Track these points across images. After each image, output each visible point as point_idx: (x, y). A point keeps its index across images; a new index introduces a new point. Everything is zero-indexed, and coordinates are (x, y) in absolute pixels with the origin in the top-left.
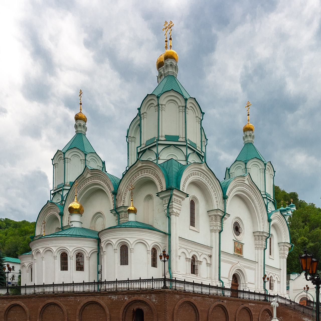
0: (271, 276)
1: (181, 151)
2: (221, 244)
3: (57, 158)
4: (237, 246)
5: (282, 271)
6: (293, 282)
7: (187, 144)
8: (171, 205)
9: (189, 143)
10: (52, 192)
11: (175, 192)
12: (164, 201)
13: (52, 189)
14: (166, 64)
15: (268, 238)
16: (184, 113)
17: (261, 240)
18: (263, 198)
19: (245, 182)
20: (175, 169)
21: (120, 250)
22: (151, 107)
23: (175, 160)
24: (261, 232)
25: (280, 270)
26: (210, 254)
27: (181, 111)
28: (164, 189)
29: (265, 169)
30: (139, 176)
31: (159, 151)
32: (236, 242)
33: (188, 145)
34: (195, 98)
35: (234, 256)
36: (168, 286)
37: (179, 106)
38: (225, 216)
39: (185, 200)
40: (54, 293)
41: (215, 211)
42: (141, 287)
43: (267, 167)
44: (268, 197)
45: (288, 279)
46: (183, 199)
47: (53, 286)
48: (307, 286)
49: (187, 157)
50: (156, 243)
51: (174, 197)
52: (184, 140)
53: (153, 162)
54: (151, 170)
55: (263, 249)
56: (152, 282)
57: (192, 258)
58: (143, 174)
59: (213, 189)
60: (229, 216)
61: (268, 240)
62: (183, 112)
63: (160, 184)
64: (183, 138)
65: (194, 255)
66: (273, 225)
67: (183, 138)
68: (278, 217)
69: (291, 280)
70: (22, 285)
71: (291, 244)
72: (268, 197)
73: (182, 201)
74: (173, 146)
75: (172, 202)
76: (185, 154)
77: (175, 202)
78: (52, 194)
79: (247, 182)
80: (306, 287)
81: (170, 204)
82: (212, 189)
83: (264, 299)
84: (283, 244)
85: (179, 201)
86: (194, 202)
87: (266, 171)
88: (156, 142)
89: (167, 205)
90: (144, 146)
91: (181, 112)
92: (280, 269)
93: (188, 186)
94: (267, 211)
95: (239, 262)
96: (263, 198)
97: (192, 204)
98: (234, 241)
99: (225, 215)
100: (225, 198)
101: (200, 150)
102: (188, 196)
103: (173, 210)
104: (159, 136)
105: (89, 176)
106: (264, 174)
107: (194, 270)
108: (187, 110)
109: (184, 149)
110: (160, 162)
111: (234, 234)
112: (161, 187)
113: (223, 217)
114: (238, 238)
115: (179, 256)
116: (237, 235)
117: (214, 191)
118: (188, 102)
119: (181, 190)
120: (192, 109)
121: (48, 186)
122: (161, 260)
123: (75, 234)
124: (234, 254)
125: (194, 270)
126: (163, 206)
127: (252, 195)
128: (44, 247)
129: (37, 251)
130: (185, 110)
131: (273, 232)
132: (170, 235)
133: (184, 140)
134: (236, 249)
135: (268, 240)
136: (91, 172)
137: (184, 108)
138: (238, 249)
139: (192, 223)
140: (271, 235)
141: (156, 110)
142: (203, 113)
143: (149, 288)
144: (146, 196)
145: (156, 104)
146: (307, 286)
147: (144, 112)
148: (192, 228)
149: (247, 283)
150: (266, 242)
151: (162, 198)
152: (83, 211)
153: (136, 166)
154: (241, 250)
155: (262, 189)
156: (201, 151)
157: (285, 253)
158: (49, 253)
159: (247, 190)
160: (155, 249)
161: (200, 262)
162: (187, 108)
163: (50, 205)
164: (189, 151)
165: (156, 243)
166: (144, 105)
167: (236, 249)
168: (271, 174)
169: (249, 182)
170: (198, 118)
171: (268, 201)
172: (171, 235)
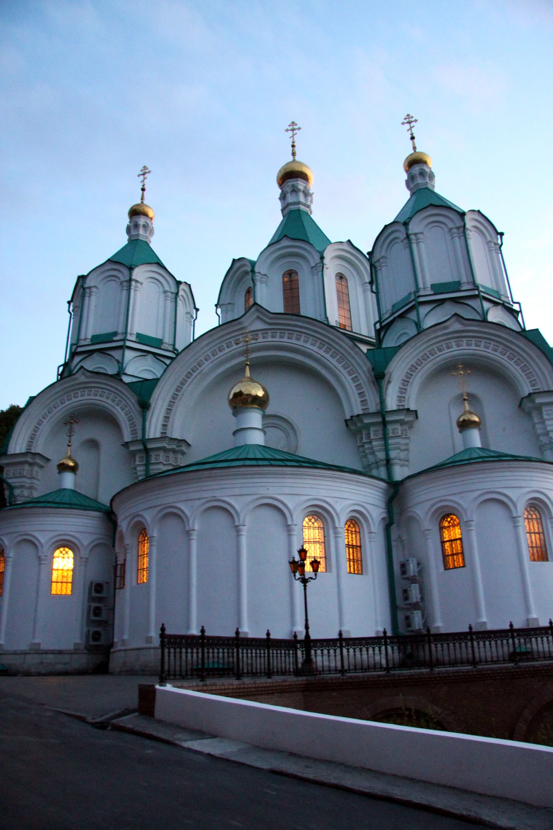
1: (469, 308)
7: (479, 293)
9: (483, 290)
14: (412, 174)
16: (462, 238)
27: (455, 236)
31: (422, 316)
33: (482, 294)
34: (479, 211)
37: (450, 229)
52: (471, 287)
64: (468, 283)
67: (169, 345)
70: (389, 409)
88: (413, 300)
90: (388, 315)
91: (457, 239)
104: (126, 333)
108: (468, 232)
121: (73, 305)
122: (295, 578)
123: (294, 453)
128: (156, 506)
129: (136, 519)
142: (502, 234)
145: (403, 236)
158: (173, 523)
164: (486, 305)
172: (346, 426)
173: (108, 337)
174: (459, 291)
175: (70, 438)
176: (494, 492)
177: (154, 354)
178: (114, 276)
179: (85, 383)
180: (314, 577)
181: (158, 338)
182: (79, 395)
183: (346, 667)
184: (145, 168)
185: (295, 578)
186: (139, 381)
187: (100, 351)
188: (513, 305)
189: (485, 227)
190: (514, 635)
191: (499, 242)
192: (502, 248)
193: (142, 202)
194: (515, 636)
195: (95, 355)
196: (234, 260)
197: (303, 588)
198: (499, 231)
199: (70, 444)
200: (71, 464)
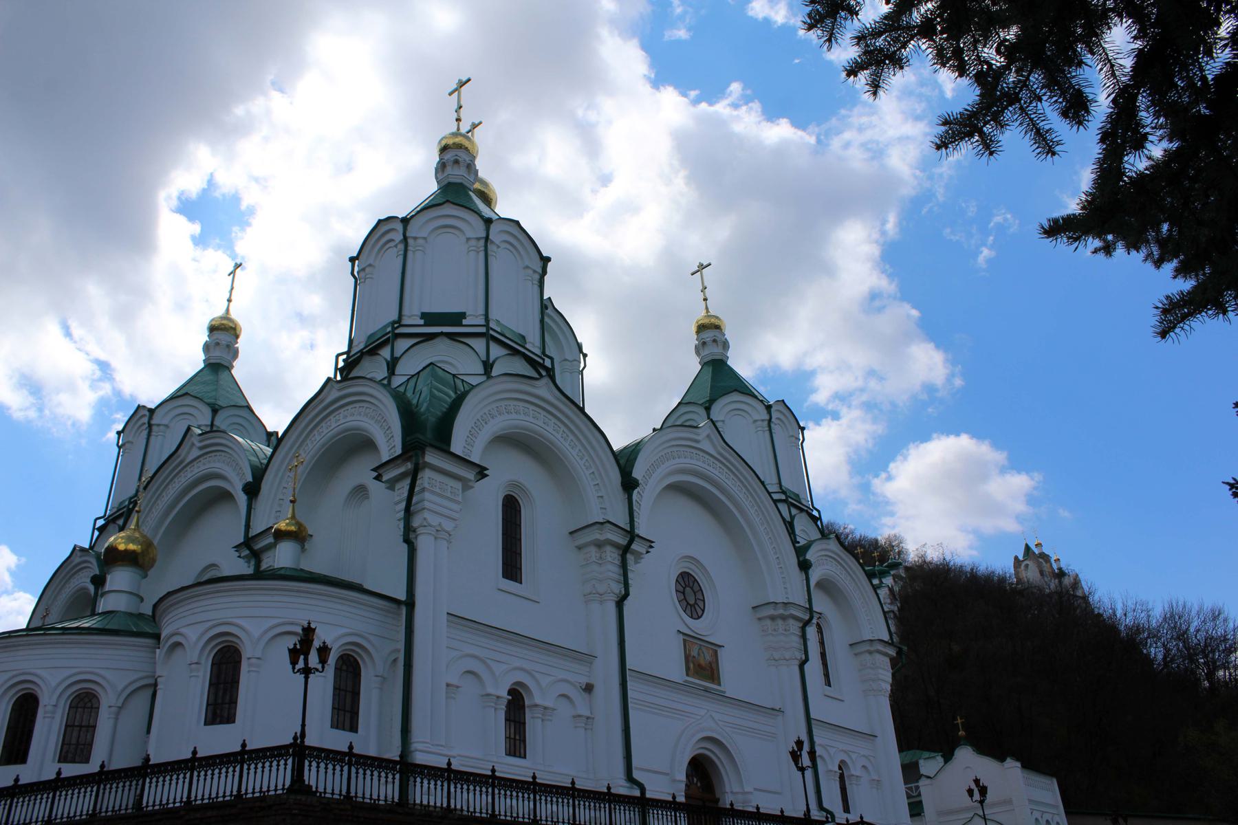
0: (843, 762)
3: (133, 427)
4: (694, 653)
6: (931, 785)
8: (417, 503)
10: (100, 523)
11: (431, 457)
13: (102, 515)
15: (807, 623)
17: (785, 630)
18: (775, 502)
21: (213, 664)
22: (387, 249)
24: (779, 605)
26: (584, 680)
28: (399, 451)
29: (770, 421)
32: (689, 640)
33: (491, 332)
34: (517, 223)
35: (683, 688)
36: (313, 783)
38: (634, 546)
41: (595, 527)
43: (774, 415)
44: (790, 500)
45: (911, 773)
46: (466, 485)
48: (977, 781)
55: (797, 663)
57: (508, 695)
59: (584, 460)
60: (651, 547)
61: (811, 631)
62: (478, 252)
66: (819, 585)
68: (834, 558)
69: (923, 779)
72: (790, 500)
75: (423, 490)
76: (484, 358)
77: (433, 493)
78: (98, 529)
79: (706, 445)
80: (973, 786)
81: (415, 499)
82: (579, 461)
84: (867, 647)
85: (450, 488)
87: (772, 425)
89: (403, 505)
93: (490, 442)
94: (794, 542)
95: (708, 711)
96: (775, 502)
97: (511, 509)
98: (681, 637)
99: (631, 542)
101: (538, 352)
102: (485, 472)
103: (425, 519)
105: (195, 453)
106: (767, 434)
107: (516, 745)
109: (479, 344)
111: (678, 613)
112: (391, 449)
113: (625, 550)
115: (448, 685)
117: (587, 464)
120: (511, 248)
122: (972, 800)
124: (686, 681)
125: (516, 745)
127: (731, 486)
130: (486, 246)
131: (821, 603)
132: (410, 604)
133: (482, 322)
134: (692, 666)
135: (811, 631)
136: (201, 441)
137: (482, 242)
138: (702, 662)
139: (512, 568)
140: (816, 616)
141: (400, 253)
144: (351, 492)
146: (977, 781)
147: (367, 264)
149: (752, 790)
150: (804, 637)
151: (392, 484)
152: (153, 561)
153: (322, 401)
155: (771, 480)
157: (881, 677)
159: (711, 469)
162: (492, 242)
163: (77, 560)
164: (496, 351)
166: (370, 245)
167: (692, 666)
168: (792, 436)
169: (714, 447)
170: (530, 272)
171: (794, 511)
174: (461, 325)
177: (451, 336)
180: (296, 671)
185: (293, 671)
189: (518, 239)
197: (303, 680)
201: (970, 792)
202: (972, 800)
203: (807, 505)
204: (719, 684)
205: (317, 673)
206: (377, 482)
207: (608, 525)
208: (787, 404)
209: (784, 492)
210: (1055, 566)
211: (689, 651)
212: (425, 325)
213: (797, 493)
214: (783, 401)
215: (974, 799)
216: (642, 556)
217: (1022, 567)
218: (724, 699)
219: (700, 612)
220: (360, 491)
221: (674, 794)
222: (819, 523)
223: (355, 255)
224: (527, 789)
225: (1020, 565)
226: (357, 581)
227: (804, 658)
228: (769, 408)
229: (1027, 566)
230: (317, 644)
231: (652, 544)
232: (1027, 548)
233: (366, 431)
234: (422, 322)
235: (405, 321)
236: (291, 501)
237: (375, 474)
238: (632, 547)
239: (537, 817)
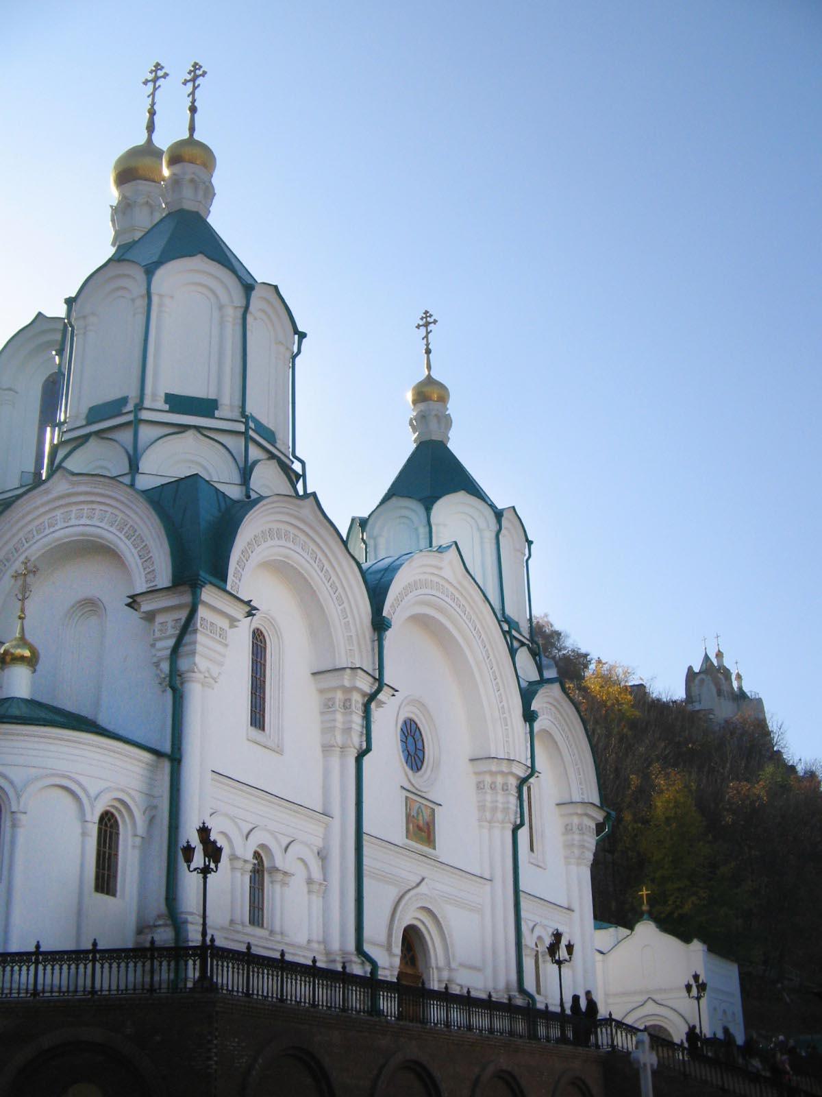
2: (364, 804)
5: (576, 915)
12: (157, 626)
19: (442, 573)
20: (207, 512)
23: (207, 481)
25: (569, 912)
30: (57, 528)
34: (276, 287)
38: (380, 696)
39: (237, 627)
40: (38, 994)
42: (98, 986)
44: (514, 633)
47: (37, 963)
49: (246, 473)
50: (123, 791)
51: (202, 612)
53: (118, 479)
54: (110, 510)
55: (511, 827)
56: (32, 968)
58: (73, 522)
60: (393, 695)
63: (142, 564)
65: (263, 846)
71: (605, 811)
73: (230, 627)
74: (196, 433)
80: (692, 982)
81: (187, 639)
83: (559, 1034)
85: (218, 630)
86: (264, 637)
87: (250, 319)
88: (130, 412)
92: (568, 909)
97: (259, 642)
100: (380, 624)
110: (144, 482)
112: (149, 573)
113: (372, 697)
114: (419, 780)
116: (412, 769)
118: (255, 294)
119: (228, 588)
122: (189, 867)
126: (153, 645)
133: (236, 414)
138: (421, 823)
139: (258, 719)
142: (302, 336)
143: (110, 990)
148: (254, 733)
151: (150, 617)
154: (429, 829)
156: (291, 457)
160: (113, 815)
161: (285, 873)
165: (123, 791)
167: (411, 826)
173: (115, 407)
174: (212, 416)
175: (23, 604)
176: (64, 776)
177: (197, 428)
178: (117, 289)
179: (69, 495)
181: (210, 397)
182: (73, 516)
183: (40, 987)
184: (158, 67)
186: (176, 481)
187: (98, 433)
188: (293, 462)
190: (96, 957)
191: (295, 350)
192: (298, 360)
193: (150, 140)
194: (98, 958)
195: (191, 433)
196: (40, 314)
197: (201, 881)
198: (300, 329)
199: (23, 616)
200: (27, 653)
201: (688, 988)
202: (689, 995)
203: (287, 454)
204: (434, 849)
205: (567, 963)
206: (129, 608)
207: (359, 671)
208: (519, 514)
209: (245, 417)
210: (735, 685)
211: (410, 809)
212: (171, 411)
213: (271, 426)
214: (514, 507)
215: (193, 866)
216: (236, 624)
217: (697, 681)
218: (443, 866)
219: (419, 764)
220: (90, 606)
221: (283, 950)
222: (300, 486)
223: (73, 295)
224: (241, 961)
225: (694, 679)
226: (85, 712)
227: (364, 746)
228: (499, 515)
229: (702, 681)
230: (564, 942)
231: (396, 693)
232: (707, 658)
233: (117, 548)
234: (167, 407)
235: (147, 404)
236: (20, 618)
237: (130, 600)
238: (378, 697)
239: (283, 996)
